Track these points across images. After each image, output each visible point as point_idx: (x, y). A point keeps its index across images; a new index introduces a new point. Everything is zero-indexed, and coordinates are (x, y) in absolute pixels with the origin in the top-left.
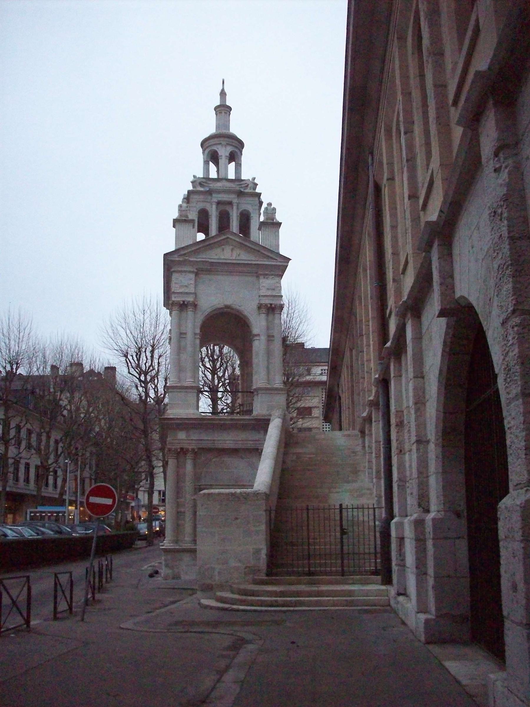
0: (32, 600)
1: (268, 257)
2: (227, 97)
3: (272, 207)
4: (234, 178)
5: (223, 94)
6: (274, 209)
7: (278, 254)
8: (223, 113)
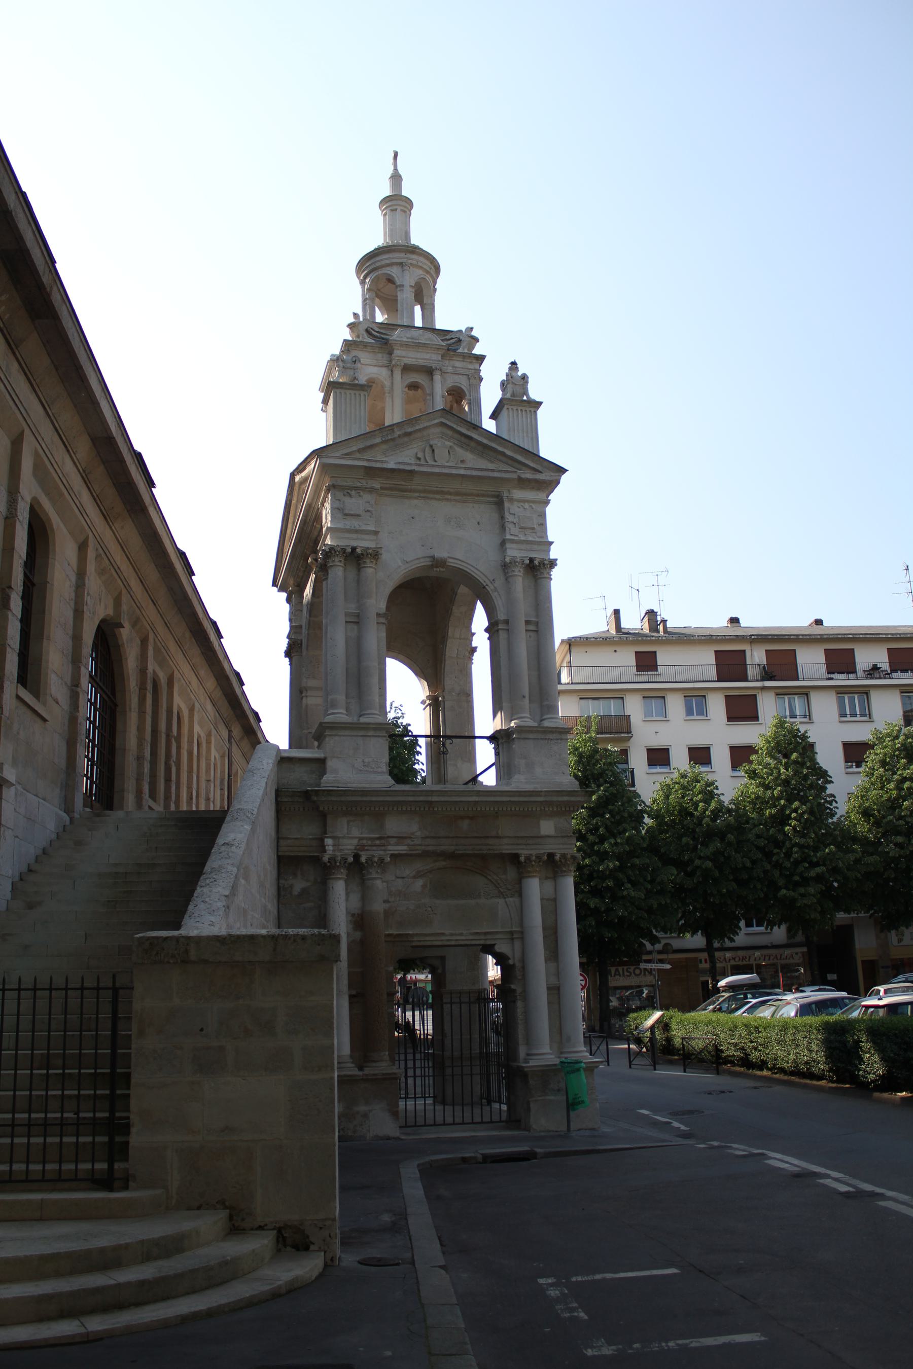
0: (609, 1051)
1: (345, 455)
2: (403, 183)
3: (520, 373)
4: (421, 326)
5: (396, 178)
6: (524, 378)
7: (536, 457)
8: (399, 210)
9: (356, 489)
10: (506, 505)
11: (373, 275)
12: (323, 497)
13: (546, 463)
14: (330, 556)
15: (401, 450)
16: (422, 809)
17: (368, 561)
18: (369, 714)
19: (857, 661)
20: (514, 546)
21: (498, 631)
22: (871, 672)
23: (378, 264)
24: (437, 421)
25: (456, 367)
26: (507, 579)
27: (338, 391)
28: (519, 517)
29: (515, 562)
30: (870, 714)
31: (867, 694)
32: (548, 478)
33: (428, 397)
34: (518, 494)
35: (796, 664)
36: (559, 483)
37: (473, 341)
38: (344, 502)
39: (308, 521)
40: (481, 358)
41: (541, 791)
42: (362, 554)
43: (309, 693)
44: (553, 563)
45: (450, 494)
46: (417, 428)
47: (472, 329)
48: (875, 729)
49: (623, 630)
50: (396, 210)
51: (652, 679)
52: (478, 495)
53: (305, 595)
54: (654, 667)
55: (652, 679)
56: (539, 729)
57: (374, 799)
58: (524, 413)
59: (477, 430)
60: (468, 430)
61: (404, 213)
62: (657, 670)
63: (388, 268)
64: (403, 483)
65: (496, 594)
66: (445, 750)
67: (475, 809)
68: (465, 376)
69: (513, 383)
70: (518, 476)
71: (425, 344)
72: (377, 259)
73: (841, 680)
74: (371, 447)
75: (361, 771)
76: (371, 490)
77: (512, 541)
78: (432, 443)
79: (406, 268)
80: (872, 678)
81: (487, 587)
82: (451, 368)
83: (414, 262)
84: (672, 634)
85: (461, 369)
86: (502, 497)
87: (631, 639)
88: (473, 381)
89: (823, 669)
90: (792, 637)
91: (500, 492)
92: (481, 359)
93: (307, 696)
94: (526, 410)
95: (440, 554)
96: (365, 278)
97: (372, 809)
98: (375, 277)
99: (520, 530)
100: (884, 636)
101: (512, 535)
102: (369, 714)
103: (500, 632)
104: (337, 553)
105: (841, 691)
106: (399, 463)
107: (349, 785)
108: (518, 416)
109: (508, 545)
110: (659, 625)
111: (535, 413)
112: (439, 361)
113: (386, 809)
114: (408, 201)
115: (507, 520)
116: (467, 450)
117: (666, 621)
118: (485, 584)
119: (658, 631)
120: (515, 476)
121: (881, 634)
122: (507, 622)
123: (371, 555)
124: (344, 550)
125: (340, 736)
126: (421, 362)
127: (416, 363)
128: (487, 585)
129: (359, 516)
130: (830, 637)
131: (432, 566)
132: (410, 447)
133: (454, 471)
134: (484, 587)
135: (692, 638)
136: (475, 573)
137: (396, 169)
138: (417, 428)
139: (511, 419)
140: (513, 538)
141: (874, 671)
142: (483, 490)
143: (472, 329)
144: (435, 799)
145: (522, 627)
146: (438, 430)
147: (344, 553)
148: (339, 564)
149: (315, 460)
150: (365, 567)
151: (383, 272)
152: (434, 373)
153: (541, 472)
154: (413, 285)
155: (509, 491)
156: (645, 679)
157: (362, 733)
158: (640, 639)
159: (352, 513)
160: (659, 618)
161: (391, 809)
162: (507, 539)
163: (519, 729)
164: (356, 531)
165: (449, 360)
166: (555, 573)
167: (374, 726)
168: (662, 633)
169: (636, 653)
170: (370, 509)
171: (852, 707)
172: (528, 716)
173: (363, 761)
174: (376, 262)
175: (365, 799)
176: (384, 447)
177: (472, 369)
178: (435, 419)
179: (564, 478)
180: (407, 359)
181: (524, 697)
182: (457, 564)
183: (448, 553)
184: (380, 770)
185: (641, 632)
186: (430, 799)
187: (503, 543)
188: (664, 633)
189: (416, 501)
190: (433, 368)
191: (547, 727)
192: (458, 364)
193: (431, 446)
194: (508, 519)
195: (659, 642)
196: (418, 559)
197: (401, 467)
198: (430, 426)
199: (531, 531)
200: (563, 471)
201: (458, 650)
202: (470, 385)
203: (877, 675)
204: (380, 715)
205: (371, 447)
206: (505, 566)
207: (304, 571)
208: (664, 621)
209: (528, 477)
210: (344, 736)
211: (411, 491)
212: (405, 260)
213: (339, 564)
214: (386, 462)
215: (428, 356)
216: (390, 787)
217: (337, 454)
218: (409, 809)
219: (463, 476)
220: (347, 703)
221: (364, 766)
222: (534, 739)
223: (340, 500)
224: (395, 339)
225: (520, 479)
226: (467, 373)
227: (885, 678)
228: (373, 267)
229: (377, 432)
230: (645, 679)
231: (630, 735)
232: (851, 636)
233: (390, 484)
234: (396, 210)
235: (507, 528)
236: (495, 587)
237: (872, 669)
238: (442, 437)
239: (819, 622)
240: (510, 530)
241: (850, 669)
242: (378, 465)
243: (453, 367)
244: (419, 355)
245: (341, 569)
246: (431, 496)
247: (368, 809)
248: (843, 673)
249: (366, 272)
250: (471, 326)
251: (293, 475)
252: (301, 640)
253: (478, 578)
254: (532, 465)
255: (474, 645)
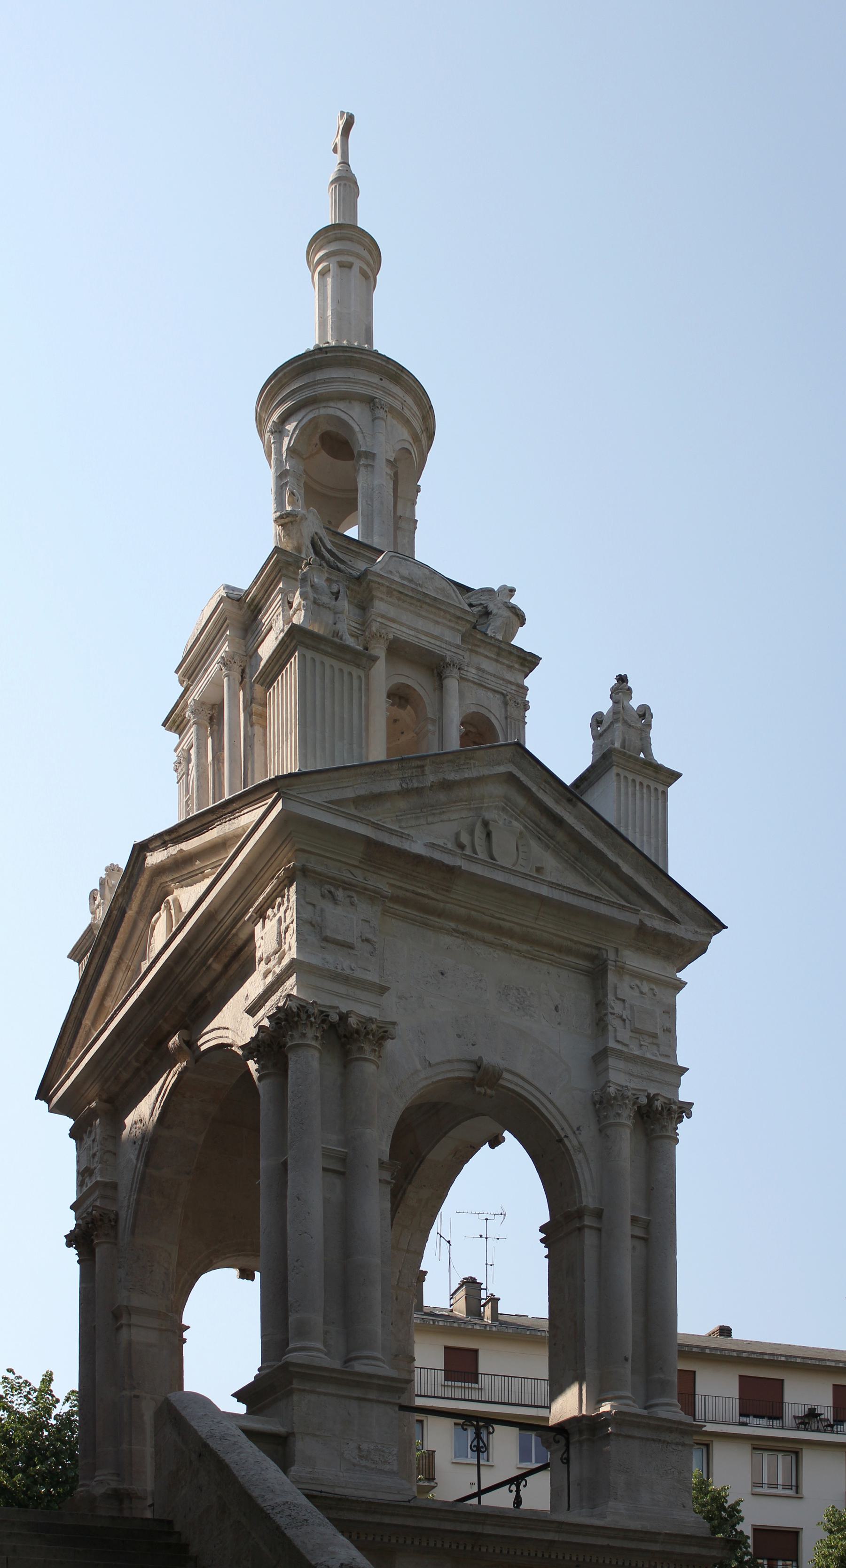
2: (360, 201)
6: (645, 713)
8: (355, 269)
9: (347, 886)
10: (611, 978)
11: (307, 415)
12: (269, 895)
13: (690, 905)
14: (296, 1023)
15: (430, 819)
16: (461, 1547)
17: (367, 1047)
18: (368, 1358)
19: (787, 1398)
20: (621, 1065)
21: (580, 1229)
22: (806, 1421)
23: (321, 390)
24: (502, 769)
25: (483, 671)
26: (603, 1130)
27: (309, 654)
28: (632, 1007)
29: (624, 1097)
30: (797, 1487)
31: (797, 1454)
32: (689, 936)
33: (430, 727)
34: (634, 960)
35: (694, 1394)
36: (704, 951)
37: (515, 619)
38: (322, 910)
39: (192, 952)
40: (531, 662)
41: (659, 1534)
42: (357, 1032)
43: (135, 1319)
44: (685, 1109)
45: (511, 934)
46: (467, 775)
47: (512, 591)
48: (833, 1507)
49: (425, 1310)
50: (350, 266)
51: (470, 1395)
52: (560, 949)
53: (129, 1121)
54: (472, 1375)
55: (470, 1395)
56: (652, 1422)
57: (387, 1520)
58: (645, 790)
59: (575, 806)
60: (557, 802)
61: (363, 279)
62: (477, 1382)
63: (341, 405)
64: (433, 895)
65: (581, 1156)
66: (481, 1444)
67: (546, 1556)
68: (498, 696)
69: (625, 722)
70: (641, 921)
71: (435, 599)
72: (320, 375)
73: (759, 1428)
74: (377, 798)
75: (354, 1465)
76: (374, 896)
77: (619, 1054)
78: (488, 815)
79: (380, 413)
80: (806, 1430)
81: (566, 1141)
82: (474, 671)
83: (397, 405)
84: (502, 1323)
85: (493, 679)
86: (606, 961)
87: (441, 1323)
88: (512, 710)
89: (734, 1408)
90: (694, 1350)
91: (599, 949)
92: (529, 661)
93: (129, 1325)
94: (648, 786)
95: (492, 1058)
96: (284, 419)
97: (378, 1539)
98: (310, 421)
99: (633, 1035)
100: (833, 1364)
101: (618, 1041)
102: (368, 1358)
103: (587, 1232)
104: (312, 1019)
105: (760, 1445)
106: (433, 846)
107: (338, 1490)
108: (634, 794)
109: (612, 1061)
110: (484, 1305)
111: (665, 794)
112: (458, 647)
113: (401, 1541)
114: (375, 253)
115: (610, 1010)
116: (547, 847)
117: (499, 1299)
118: (563, 1135)
119: (480, 1316)
120: (634, 920)
121: (828, 1360)
122: (599, 1214)
123: (373, 1035)
124: (324, 1016)
125: (319, 1393)
126: (425, 642)
127: (415, 641)
128: (566, 1136)
129: (351, 947)
130: (753, 1356)
131: (470, 1083)
132: (445, 817)
133: (531, 887)
134: (560, 1141)
135: (539, 1334)
136: (547, 1109)
137: (345, 162)
138: (466, 776)
139: (622, 798)
140: (619, 1047)
141: (809, 1419)
142: (571, 940)
143: (512, 591)
144: (488, 1530)
145: (627, 1229)
146: (498, 790)
147: (323, 1021)
148: (313, 1043)
149: (270, 801)
150: (357, 1059)
151: (330, 411)
152: (447, 672)
153: (678, 922)
154: (392, 460)
155: (617, 950)
156: (460, 1394)
157: (356, 1393)
158: (456, 1325)
159: (339, 937)
160: (483, 1294)
161: (409, 1542)
162: (613, 1049)
163: (619, 1418)
164: (346, 980)
165: (471, 651)
166: (684, 1128)
167: (381, 1382)
168: (488, 1320)
169: (447, 1349)
170: (370, 936)
171: (774, 1473)
172: (630, 1395)
173: (359, 1448)
174: (316, 383)
175: (370, 1518)
176: (402, 804)
177: (510, 683)
178: (499, 764)
179: (717, 941)
180: (398, 627)
181: (626, 1359)
182: (517, 1084)
183: (503, 1059)
184: (387, 1467)
185: (451, 1314)
186: (479, 1529)
187: (600, 1057)
188: (492, 1320)
189: (447, 940)
190: (448, 660)
191: (665, 1420)
192: (486, 665)
193: (486, 824)
194: (613, 1008)
195: (485, 1334)
196: (449, 1061)
197: (437, 855)
198: (489, 776)
199: (651, 1040)
200: (717, 926)
201: (400, 1272)
202: (506, 718)
203: (814, 1426)
204: (383, 1362)
205: (377, 798)
206: (601, 1103)
207: (138, 1070)
208: (494, 1301)
209: (658, 927)
210: (326, 1394)
211: (440, 914)
212: (378, 394)
213: (313, 1043)
214: (408, 837)
215: (437, 630)
216: (409, 1501)
217: (318, 799)
218: (439, 1545)
219: (543, 900)
220: (326, 1333)
221: (361, 1457)
222: (641, 1438)
223: (314, 905)
224: (378, 571)
225: (642, 930)
226: (503, 689)
227: (825, 1431)
228: (307, 394)
229: (395, 767)
230: (460, 1394)
231: (433, 1484)
232: (783, 1359)
233: (407, 890)
234: (350, 266)
235: (610, 1027)
236: (579, 1143)
237: (806, 1416)
238: (504, 809)
239: (725, 1331)
240: (615, 1030)
241: (775, 1413)
242: (394, 842)
243: (479, 669)
244: (420, 624)
245: (317, 1054)
246: (476, 932)
247: (370, 1538)
248: (762, 1417)
249: (288, 404)
250: (510, 585)
251: (140, 850)
252: (117, 1214)
253: (552, 1120)
254: (664, 903)
255: (423, 1268)
